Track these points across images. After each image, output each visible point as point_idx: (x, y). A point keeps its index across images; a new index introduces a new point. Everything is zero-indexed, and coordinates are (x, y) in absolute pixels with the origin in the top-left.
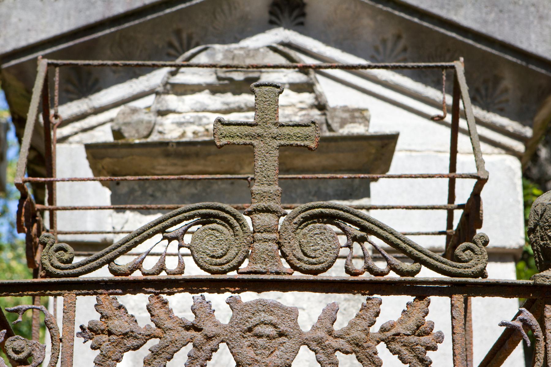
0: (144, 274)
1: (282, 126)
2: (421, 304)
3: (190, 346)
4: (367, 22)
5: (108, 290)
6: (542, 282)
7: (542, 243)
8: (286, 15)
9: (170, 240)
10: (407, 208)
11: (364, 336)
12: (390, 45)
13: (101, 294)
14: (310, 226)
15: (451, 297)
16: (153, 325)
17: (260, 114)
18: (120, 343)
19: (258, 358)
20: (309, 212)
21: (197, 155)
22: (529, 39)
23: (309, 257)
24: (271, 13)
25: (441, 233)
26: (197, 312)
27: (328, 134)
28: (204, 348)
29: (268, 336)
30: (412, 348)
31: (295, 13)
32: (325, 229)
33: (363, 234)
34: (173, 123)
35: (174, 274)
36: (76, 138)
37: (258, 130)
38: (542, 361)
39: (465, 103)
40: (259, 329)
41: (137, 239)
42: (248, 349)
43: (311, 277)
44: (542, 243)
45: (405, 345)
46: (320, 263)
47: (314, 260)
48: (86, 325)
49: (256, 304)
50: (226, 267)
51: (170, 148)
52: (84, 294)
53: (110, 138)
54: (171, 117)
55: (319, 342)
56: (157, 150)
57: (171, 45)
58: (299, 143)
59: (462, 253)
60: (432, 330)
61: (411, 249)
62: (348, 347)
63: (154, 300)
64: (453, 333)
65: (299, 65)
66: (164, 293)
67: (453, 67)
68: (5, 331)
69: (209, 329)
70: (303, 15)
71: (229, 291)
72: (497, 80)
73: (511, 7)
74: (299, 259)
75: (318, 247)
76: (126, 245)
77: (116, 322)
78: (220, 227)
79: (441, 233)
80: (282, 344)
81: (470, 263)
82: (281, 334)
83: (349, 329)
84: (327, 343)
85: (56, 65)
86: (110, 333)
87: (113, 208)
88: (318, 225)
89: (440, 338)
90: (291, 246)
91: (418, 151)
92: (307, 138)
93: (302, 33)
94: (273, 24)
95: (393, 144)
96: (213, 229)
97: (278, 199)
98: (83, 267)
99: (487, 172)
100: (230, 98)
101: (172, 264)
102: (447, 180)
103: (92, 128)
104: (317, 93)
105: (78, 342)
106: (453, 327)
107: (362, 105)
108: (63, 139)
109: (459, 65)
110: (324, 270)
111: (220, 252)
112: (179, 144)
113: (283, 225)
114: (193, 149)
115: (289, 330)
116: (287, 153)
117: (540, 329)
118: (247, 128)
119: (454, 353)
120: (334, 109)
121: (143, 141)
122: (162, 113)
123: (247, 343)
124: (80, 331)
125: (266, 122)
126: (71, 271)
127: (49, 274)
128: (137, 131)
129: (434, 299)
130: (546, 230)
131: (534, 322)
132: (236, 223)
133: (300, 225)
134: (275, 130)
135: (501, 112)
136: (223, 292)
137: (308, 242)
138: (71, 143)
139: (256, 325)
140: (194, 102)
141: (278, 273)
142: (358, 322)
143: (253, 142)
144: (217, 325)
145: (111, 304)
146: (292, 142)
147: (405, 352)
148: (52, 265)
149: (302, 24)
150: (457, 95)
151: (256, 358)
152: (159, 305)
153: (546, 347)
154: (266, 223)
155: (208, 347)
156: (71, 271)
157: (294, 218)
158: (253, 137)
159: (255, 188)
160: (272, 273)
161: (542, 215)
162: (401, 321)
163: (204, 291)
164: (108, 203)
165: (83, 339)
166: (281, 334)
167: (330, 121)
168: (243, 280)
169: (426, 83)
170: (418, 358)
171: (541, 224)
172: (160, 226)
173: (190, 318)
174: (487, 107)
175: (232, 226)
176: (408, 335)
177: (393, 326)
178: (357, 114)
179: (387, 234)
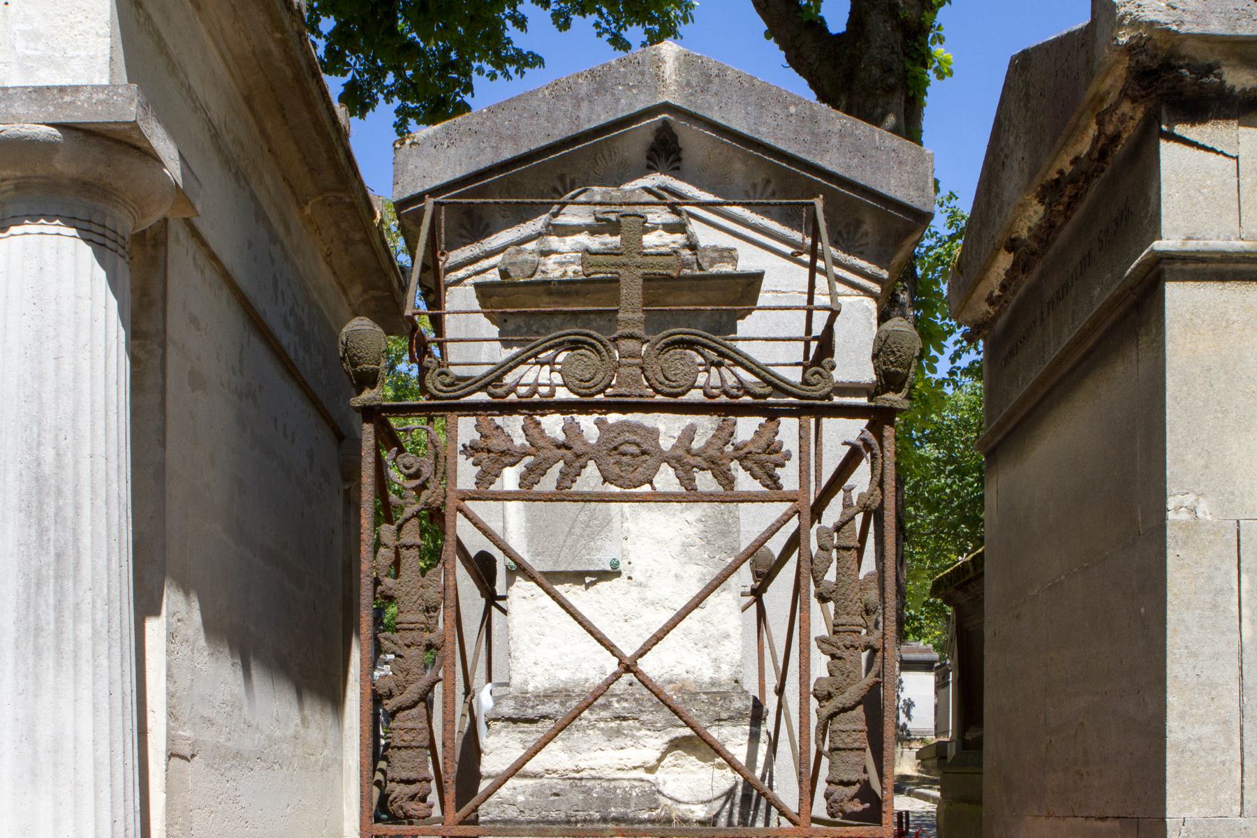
0: (519, 397)
1: (646, 255)
2: (772, 425)
3: (562, 462)
4: (738, 166)
5: (486, 411)
6: (882, 404)
7: (884, 368)
8: (663, 160)
9: (542, 364)
10: (766, 340)
11: (719, 454)
12: (759, 189)
13: (480, 415)
14: (672, 352)
15: (799, 418)
16: (527, 444)
17: (625, 244)
18: (498, 460)
19: (623, 474)
20: (670, 338)
21: (577, 293)
22: (888, 184)
23: (670, 381)
24: (648, 158)
25: (797, 364)
26: (568, 432)
27: (698, 273)
28: (574, 465)
29: (632, 454)
30: (762, 465)
31: (671, 158)
32: (685, 354)
33: (720, 359)
34: (555, 263)
35: (546, 397)
36: (470, 281)
37: (623, 259)
38: (879, 476)
39: (824, 245)
40: (624, 448)
41: (511, 364)
42: (614, 466)
43: (672, 400)
44: (884, 368)
45: (756, 463)
46: (680, 387)
47: (674, 384)
48: (468, 444)
49: (622, 425)
50: (593, 390)
51: (552, 286)
52: (465, 416)
53: (498, 278)
54: (554, 257)
55: (678, 460)
56: (540, 289)
58: (661, 272)
59: (811, 377)
60: (781, 448)
61: (764, 373)
62: (704, 464)
63: (529, 421)
64: (800, 452)
65: (668, 202)
66: (537, 415)
67: (813, 204)
68: (396, 448)
69: (578, 447)
70: (679, 160)
71: (596, 412)
72: (859, 223)
73: (873, 152)
74: (660, 383)
75: (678, 372)
76: (502, 369)
77: (495, 441)
78: (588, 353)
79: (797, 364)
80: (644, 461)
81: (818, 387)
82: (644, 453)
83: (706, 448)
84: (685, 460)
85: (442, 204)
86: (489, 451)
87: (499, 340)
88: (679, 350)
89: (788, 456)
90: (653, 371)
91: (784, 292)
92: (669, 266)
93: (676, 178)
94: (650, 169)
95: (758, 283)
96: (581, 355)
97: (642, 326)
98: (463, 391)
99: (840, 304)
102: (805, 312)
104: (689, 233)
105: (461, 459)
106: (800, 446)
107: (732, 246)
108: (458, 282)
109: (819, 203)
110: (683, 393)
111: (588, 376)
112: (560, 282)
113: (647, 351)
114: (574, 287)
115: (651, 448)
116: (660, 291)
117: (878, 447)
118: (613, 257)
119: (800, 469)
120: (705, 249)
121: (529, 280)
122: (546, 253)
123: (612, 461)
124: (462, 449)
125: (630, 252)
126: (453, 394)
127: (433, 397)
128: (522, 271)
129: (782, 420)
130: (888, 355)
131: (874, 441)
132: (602, 349)
133: (662, 350)
134: (639, 259)
135: (861, 255)
136: (591, 413)
137: (669, 367)
138: (465, 286)
139: (621, 444)
140: (574, 242)
141: (641, 396)
142: (714, 441)
143: (618, 271)
144: (586, 444)
145: (490, 424)
146: (655, 271)
147: (756, 469)
148: (435, 388)
149: (678, 168)
150: (816, 236)
151: (621, 474)
152: (532, 426)
153: (883, 464)
154: (630, 349)
155: (577, 464)
156: (453, 394)
157: (656, 344)
158: (619, 266)
159: (620, 316)
160: (635, 396)
161: (885, 341)
162: (753, 441)
163: (573, 413)
164: (497, 336)
165: (465, 456)
166: (644, 453)
167: (700, 261)
168: (609, 403)
170: (768, 474)
171: (884, 349)
172: (533, 351)
173: (561, 437)
174: (848, 251)
175: (599, 352)
176: (759, 453)
177: (745, 445)
178: (725, 254)
179: (742, 359)
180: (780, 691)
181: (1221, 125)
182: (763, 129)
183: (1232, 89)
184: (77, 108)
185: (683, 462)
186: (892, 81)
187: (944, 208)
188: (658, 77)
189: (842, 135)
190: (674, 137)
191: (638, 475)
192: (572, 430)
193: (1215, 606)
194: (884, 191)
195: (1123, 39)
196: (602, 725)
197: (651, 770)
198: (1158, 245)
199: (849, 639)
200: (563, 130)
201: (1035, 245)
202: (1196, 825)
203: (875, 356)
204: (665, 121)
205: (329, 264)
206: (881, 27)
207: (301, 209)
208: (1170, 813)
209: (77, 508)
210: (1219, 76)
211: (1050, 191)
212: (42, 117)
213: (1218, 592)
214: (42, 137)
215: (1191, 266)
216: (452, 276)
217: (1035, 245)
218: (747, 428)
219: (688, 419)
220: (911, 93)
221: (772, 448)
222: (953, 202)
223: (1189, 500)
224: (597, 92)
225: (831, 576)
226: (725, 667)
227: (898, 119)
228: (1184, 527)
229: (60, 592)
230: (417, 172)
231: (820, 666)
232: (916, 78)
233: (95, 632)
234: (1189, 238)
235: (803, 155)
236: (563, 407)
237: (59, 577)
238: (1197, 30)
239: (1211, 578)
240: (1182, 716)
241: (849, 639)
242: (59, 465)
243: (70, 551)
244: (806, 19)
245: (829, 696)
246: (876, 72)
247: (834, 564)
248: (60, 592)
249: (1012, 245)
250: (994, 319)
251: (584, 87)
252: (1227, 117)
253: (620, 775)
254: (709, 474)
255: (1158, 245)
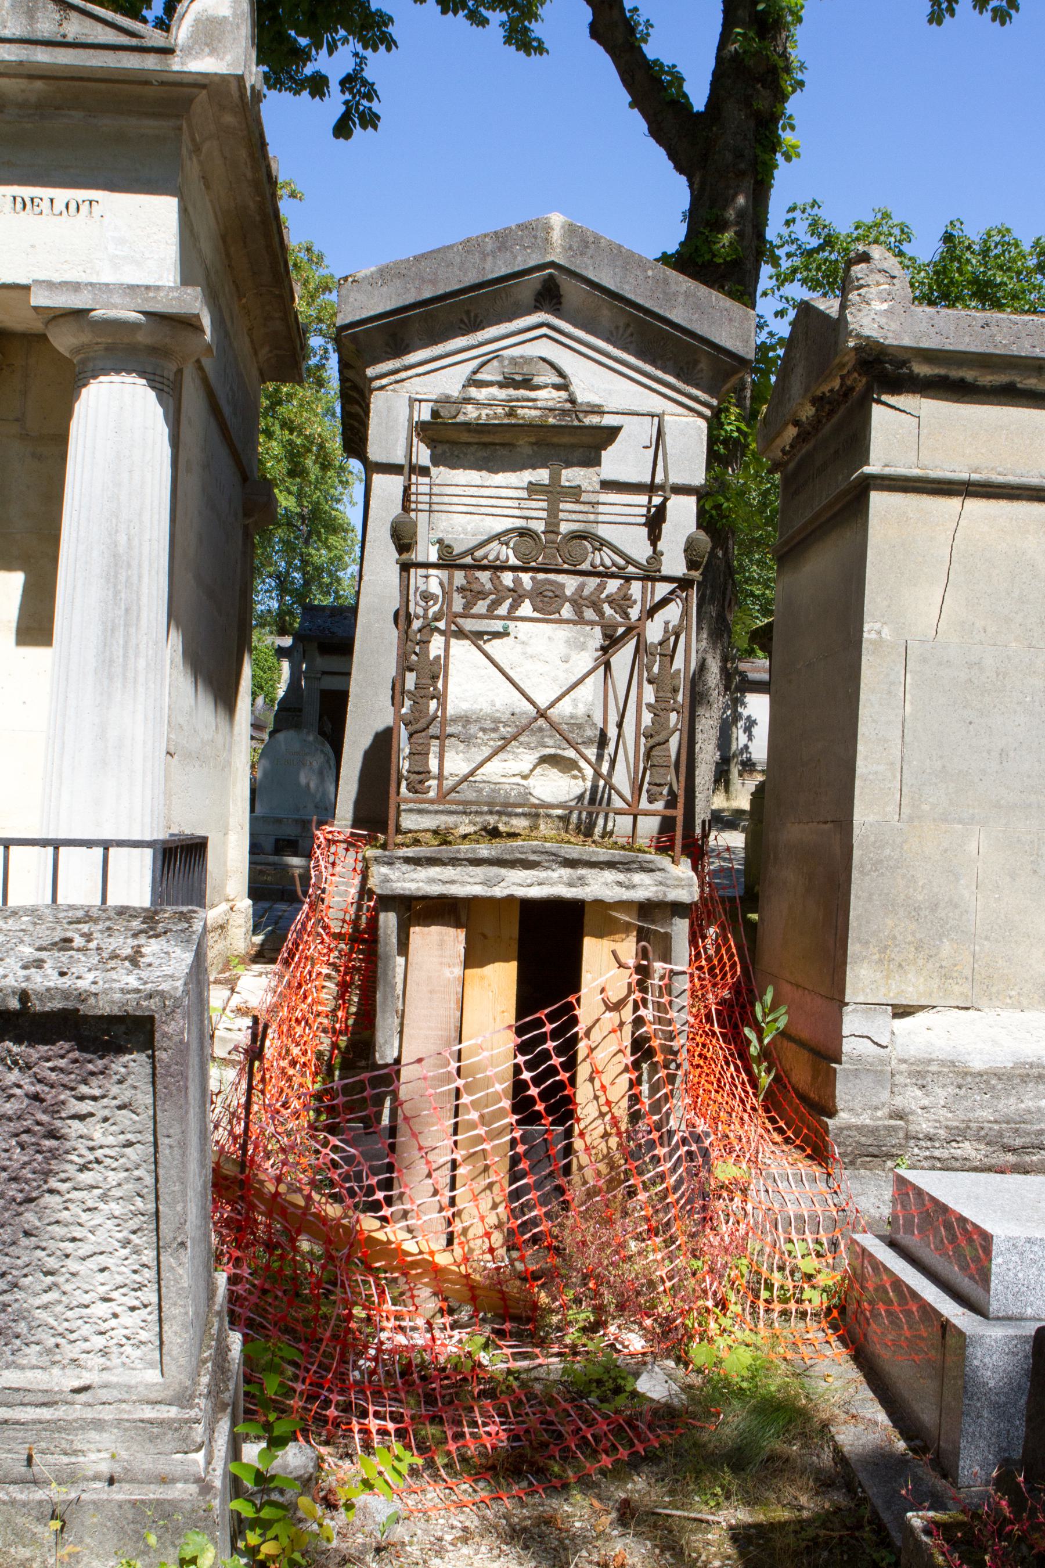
4: (606, 312)
12: (621, 330)
21: (489, 432)
24: (536, 300)
30: (620, 606)
55: (575, 601)
57: (462, 321)
69: (520, 592)
70: (560, 303)
72: (696, 362)
89: (635, 602)
94: (537, 308)
100: (511, 392)
101: (503, 557)
103: (403, 380)
105: (455, 595)
135: (697, 386)
169: (645, 362)
173: (511, 585)
180: (620, 725)
181: (910, 396)
182: (626, 287)
183: (918, 375)
184: (158, 302)
185: (577, 603)
186: (742, 166)
187: (806, 215)
188: (547, 241)
189: (687, 295)
190: (557, 287)
191: (552, 609)
192: (517, 581)
193: (889, 692)
194: (717, 341)
195: (851, 344)
196: (492, 743)
197: (525, 777)
198: (867, 469)
199: (663, 705)
200: (471, 279)
201: (810, 429)
202: (871, 825)
203: (685, 551)
204: (551, 275)
205: (250, 335)
206: (735, 115)
207: (240, 299)
208: (856, 817)
209: (140, 577)
210: (910, 368)
211: (818, 401)
212: (133, 306)
213: (892, 683)
214: (132, 319)
215: (887, 482)
216: (377, 384)
217: (810, 429)
218: (613, 586)
219: (581, 579)
220: (759, 177)
221: (627, 598)
222: (816, 210)
223: (877, 626)
224: (500, 249)
225: (656, 669)
226: (581, 706)
227: (747, 201)
228: (872, 642)
229: (127, 636)
230: (356, 304)
231: (647, 718)
232: (765, 163)
233: (148, 665)
234: (886, 466)
235: (656, 310)
236: (514, 569)
237: (127, 625)
238: (895, 343)
239: (888, 675)
240: (866, 758)
241: (663, 705)
242: (130, 547)
243: (135, 607)
244: (668, 99)
245: (652, 736)
246: (729, 157)
247: (657, 664)
248: (127, 636)
249: (797, 423)
250: (787, 463)
251: (490, 245)
252: (914, 392)
253: (503, 780)
254: (591, 610)
255: (867, 469)
